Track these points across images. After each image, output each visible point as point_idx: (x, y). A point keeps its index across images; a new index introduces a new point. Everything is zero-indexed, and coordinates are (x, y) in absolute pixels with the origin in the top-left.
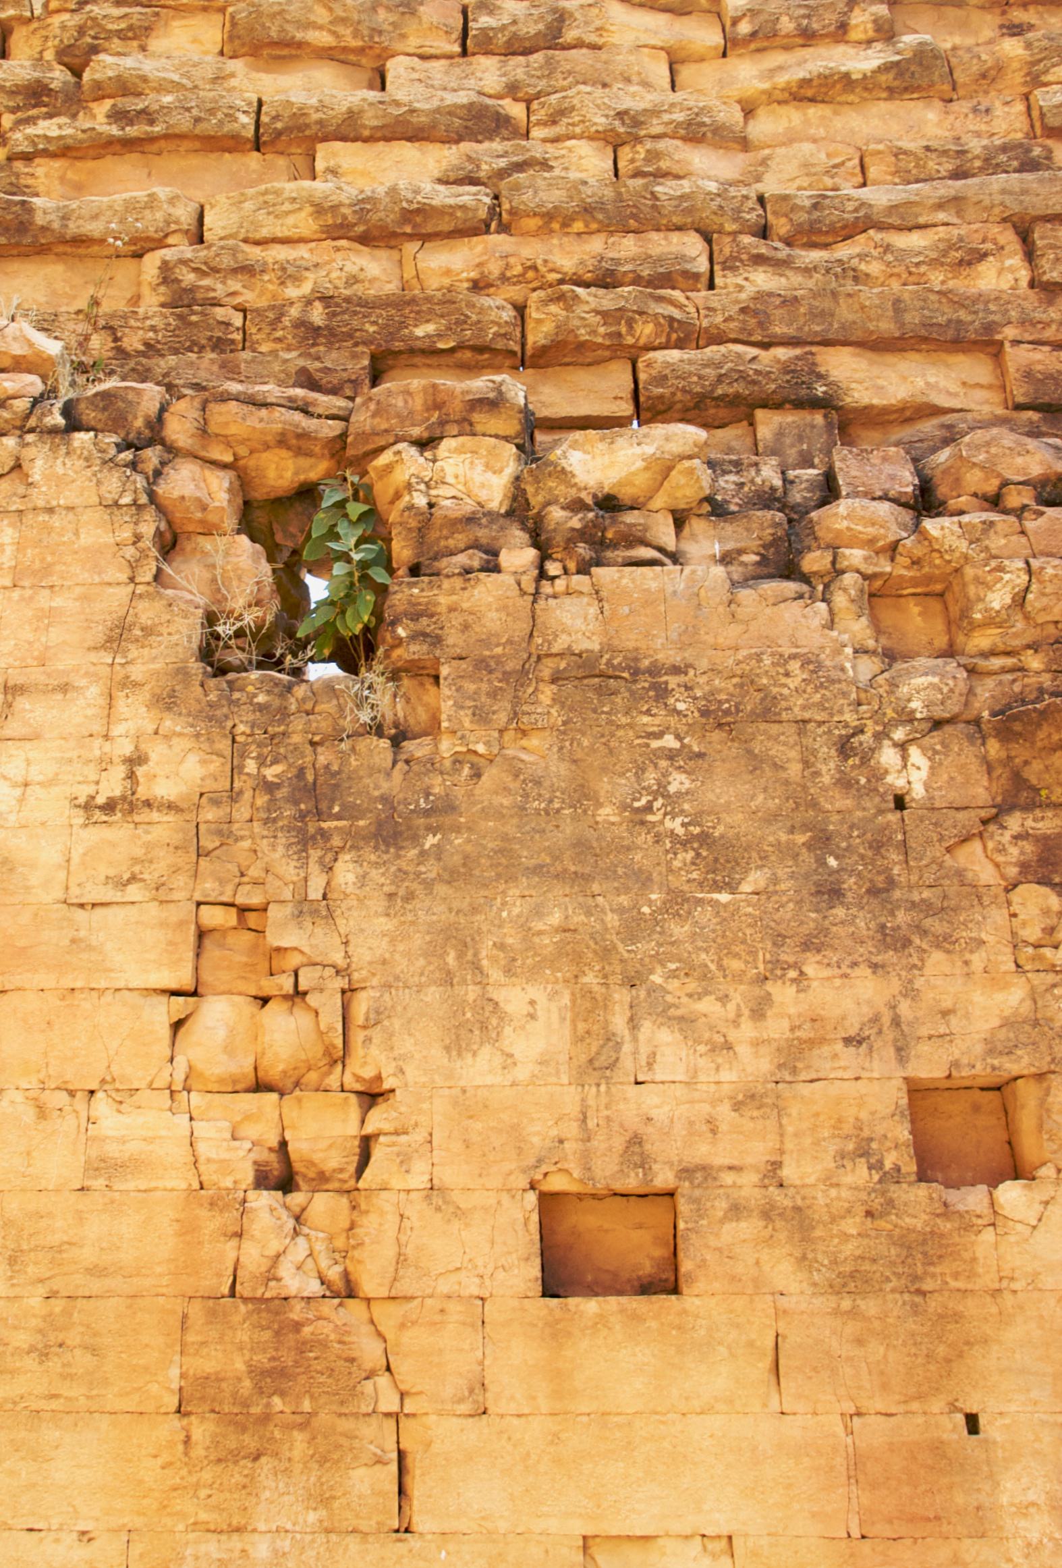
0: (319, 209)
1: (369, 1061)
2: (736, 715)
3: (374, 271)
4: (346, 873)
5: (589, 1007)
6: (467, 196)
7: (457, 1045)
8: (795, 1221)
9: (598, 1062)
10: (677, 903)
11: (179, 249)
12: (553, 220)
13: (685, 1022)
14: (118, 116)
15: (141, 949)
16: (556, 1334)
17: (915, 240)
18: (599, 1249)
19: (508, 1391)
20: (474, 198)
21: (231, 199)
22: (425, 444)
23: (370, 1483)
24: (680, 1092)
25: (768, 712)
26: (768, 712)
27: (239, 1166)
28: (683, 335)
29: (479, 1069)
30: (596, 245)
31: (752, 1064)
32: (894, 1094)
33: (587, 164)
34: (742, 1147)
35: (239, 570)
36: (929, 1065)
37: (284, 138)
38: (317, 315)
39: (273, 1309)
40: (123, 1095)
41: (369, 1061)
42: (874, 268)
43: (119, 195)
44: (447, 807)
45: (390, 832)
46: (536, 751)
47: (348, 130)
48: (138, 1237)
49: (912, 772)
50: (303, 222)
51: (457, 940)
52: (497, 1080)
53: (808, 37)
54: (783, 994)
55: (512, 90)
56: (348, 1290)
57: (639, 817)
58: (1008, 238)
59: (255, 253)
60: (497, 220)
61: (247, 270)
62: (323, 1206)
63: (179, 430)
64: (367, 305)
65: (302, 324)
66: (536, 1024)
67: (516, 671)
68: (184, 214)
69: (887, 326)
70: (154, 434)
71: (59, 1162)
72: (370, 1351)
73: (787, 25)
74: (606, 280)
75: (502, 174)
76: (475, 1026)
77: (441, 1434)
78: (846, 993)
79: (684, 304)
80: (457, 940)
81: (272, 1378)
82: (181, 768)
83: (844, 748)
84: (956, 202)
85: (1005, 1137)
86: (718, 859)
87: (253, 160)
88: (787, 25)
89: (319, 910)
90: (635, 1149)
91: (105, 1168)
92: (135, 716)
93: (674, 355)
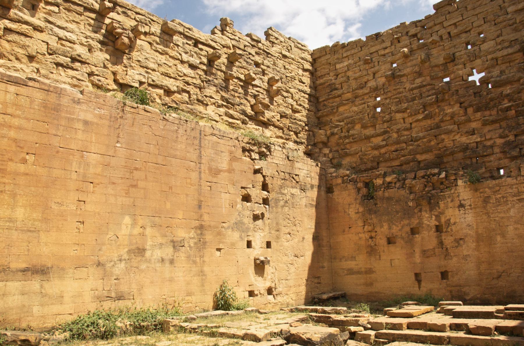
0: (371, 147)
1: (376, 229)
2: (398, 201)
3: (376, 152)
4: (373, 216)
5: (389, 224)
6: (384, 143)
7: (381, 228)
8: (403, 238)
9: (390, 228)
10: (395, 216)
11: (360, 153)
12: (392, 145)
13: (395, 225)
14: (353, 139)
15: (360, 223)
16: (388, 247)
17: (425, 140)
18: (390, 241)
19: (385, 251)
20: (384, 143)
21: (364, 147)
22: (376, 179)
23: (378, 257)
24: (395, 230)
25: (400, 200)
26: (400, 200)
27: (368, 237)
28: (403, 156)
29: (382, 229)
30: (396, 146)
31: (400, 227)
32: (409, 229)
33: (395, 135)
34: (399, 234)
35: (364, 191)
36: (412, 227)
37: (368, 138)
38: (372, 159)
39: (371, 247)
40: (361, 233)
41: (376, 229)
42: (421, 144)
43: (355, 148)
44: (379, 210)
45: (375, 212)
46: (385, 205)
47: (373, 136)
48: (363, 242)
49: (411, 204)
50: (370, 149)
51: (380, 220)
52: (384, 230)
53: (415, 114)
54: (402, 222)
55: (388, 127)
56: (376, 245)
57: (392, 210)
58: (434, 138)
59: (366, 153)
60: (387, 145)
61: (366, 155)
62: (374, 239)
63: (358, 180)
64: (376, 157)
65: (371, 160)
66: (386, 226)
67: (383, 199)
68: (360, 149)
69: (421, 152)
70: (356, 181)
71: (357, 238)
72: (377, 249)
73: (413, 114)
74: (397, 151)
75: (387, 139)
76: (382, 226)
77: (382, 254)
78: (406, 222)
79: (403, 152)
80: (380, 220)
81: (371, 251)
82: (361, 210)
83: (406, 203)
84: (429, 135)
85: (20, 274)
86: (397, 212)
87: (365, 141)
88: (413, 114)
89: (371, 219)
90: (393, 234)
91: (360, 238)
92: (358, 206)
93: (402, 158)
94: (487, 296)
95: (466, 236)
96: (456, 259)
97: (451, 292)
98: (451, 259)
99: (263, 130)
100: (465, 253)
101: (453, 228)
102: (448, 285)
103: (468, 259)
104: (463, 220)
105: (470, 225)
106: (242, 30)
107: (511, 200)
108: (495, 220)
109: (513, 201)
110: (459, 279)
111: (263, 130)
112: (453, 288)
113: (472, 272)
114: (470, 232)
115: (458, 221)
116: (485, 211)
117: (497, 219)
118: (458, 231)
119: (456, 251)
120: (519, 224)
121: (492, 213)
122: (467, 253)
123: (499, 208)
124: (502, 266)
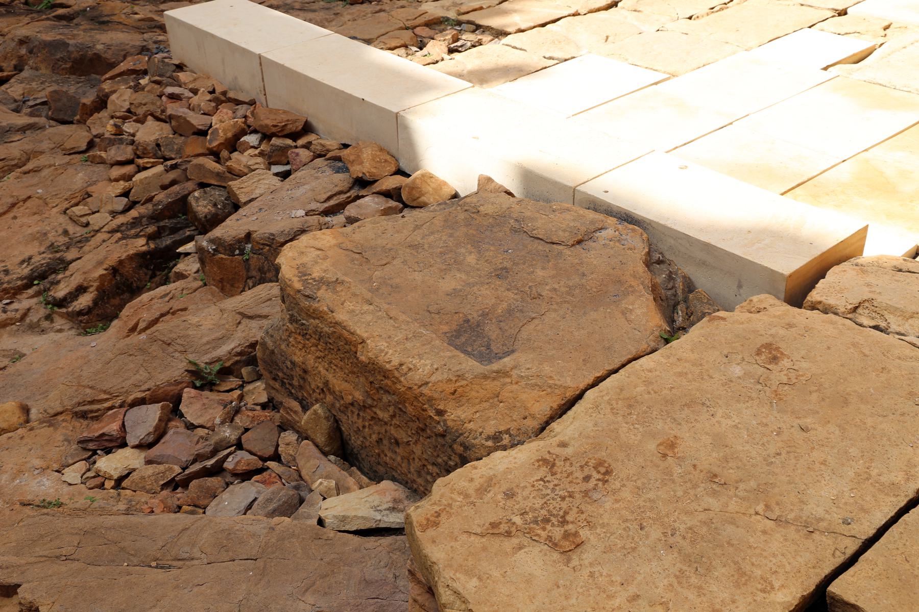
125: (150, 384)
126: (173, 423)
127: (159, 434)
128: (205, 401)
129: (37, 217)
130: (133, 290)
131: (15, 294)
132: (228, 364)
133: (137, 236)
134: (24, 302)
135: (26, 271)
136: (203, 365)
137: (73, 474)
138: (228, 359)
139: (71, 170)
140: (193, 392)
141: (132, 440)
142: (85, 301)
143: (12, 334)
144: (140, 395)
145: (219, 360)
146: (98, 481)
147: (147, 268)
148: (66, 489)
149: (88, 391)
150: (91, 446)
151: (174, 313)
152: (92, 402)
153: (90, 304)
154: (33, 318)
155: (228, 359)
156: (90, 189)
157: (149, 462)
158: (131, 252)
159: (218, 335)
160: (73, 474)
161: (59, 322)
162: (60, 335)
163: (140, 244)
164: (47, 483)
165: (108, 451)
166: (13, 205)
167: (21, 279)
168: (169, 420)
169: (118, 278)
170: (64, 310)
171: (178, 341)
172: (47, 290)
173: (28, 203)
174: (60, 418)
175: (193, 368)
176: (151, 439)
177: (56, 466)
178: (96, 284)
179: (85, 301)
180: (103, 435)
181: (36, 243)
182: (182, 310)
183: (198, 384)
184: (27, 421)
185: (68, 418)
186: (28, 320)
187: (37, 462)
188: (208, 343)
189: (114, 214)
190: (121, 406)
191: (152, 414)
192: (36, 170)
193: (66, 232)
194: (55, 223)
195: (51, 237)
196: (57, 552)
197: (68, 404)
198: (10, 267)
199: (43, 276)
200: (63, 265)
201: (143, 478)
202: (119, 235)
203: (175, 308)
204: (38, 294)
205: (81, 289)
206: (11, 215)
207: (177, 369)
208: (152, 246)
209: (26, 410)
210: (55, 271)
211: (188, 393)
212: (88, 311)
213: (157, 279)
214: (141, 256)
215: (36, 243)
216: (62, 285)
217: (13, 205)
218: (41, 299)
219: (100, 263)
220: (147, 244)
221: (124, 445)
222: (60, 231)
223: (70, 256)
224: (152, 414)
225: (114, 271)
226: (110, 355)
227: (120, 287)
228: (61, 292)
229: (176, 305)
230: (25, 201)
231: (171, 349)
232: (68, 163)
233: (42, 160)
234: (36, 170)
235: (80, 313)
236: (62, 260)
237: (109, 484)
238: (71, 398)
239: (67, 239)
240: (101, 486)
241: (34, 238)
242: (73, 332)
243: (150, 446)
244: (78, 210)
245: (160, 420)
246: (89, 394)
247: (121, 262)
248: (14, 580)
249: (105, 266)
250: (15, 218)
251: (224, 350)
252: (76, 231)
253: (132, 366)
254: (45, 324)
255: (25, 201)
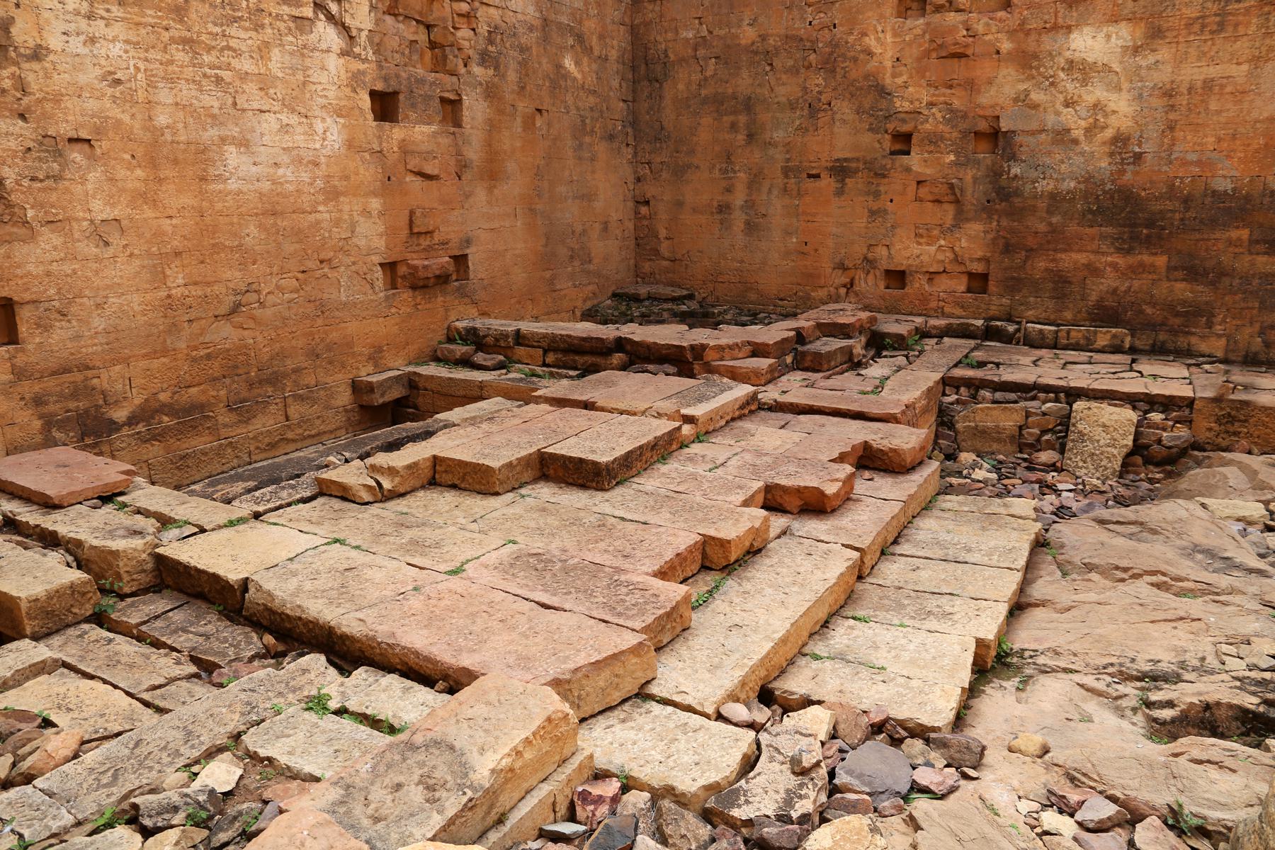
94: (193, 390)
95: (98, 130)
96: (57, 240)
97: (38, 401)
98: (33, 236)
99: (837, 480)
100: (100, 210)
101: (32, 74)
102: (20, 374)
103: (116, 240)
104: (76, 45)
105: (118, 82)
106: (977, 526)
107: (274, 12)
108: (219, 80)
109: (278, 17)
110: (78, 337)
111: (837, 480)
112: (50, 383)
113: (136, 298)
114: (116, 112)
115: (55, 42)
116: (178, 31)
117: (226, 75)
118: (57, 99)
119: (54, 197)
120: (293, 111)
121: (210, 49)
122: (108, 214)
123: (233, 30)
124: (243, 265)
125: (1133, 794)
126: (1120, 830)
127: (1100, 828)
128: (1161, 836)
129: (1192, 636)
130: (1214, 731)
131: (1126, 679)
132: (1210, 828)
133: (1254, 694)
134: (1129, 689)
135: (1147, 667)
136: (1186, 811)
137: (1025, 806)
138: (1214, 825)
139: (1252, 617)
140: (1158, 822)
141: (1079, 816)
142: (1167, 714)
143: (1099, 704)
144: (1119, 794)
145: (1204, 818)
146: (1036, 823)
147: (1243, 723)
148: (1013, 811)
149: (1089, 765)
150: (1053, 799)
151: (1221, 767)
152: (1085, 775)
153: (1168, 719)
154: (1124, 703)
155: (1214, 825)
156: (1252, 639)
157: (1075, 839)
158: (1235, 702)
159: (1223, 800)
160: (1025, 806)
161: (1139, 718)
162: (1131, 726)
163: (1250, 702)
164: (1005, 797)
165: (1061, 812)
166: (1182, 619)
167: (1138, 671)
168: (1119, 825)
169: (1207, 714)
170: (1147, 711)
171: (1184, 781)
172: (1149, 690)
173: (1194, 624)
174: (1056, 768)
175: (1176, 808)
176: (1091, 825)
177: (1021, 794)
178: (1183, 707)
179: (1167, 714)
180: (1064, 797)
181: (1173, 654)
182: (1230, 770)
183: (1170, 822)
184: (1040, 757)
185: (1061, 773)
186: (1119, 702)
187: (1016, 783)
188: (1208, 800)
189: (1252, 667)
190: (1101, 792)
191: (1108, 810)
192: (1224, 604)
193: (1203, 659)
194: (1205, 646)
195: (1188, 656)
196: (959, 833)
197: (1069, 764)
198: (1138, 659)
199: (1155, 679)
200: (1173, 678)
201: (1059, 844)
202: (1238, 684)
203: (1226, 764)
204: (1142, 689)
205: (1170, 704)
206: (1174, 624)
207: (1163, 798)
208: (1261, 709)
209: (1046, 750)
210: (1166, 681)
211: (1153, 821)
212: (1164, 723)
213: (1248, 739)
214: (1245, 711)
215: (1173, 654)
216: (1161, 693)
217: (1182, 619)
218: (1140, 693)
219: (1200, 694)
220: (1258, 705)
221: (1072, 815)
222: (1200, 655)
223: (1187, 676)
224: (1110, 810)
225: (1207, 707)
226: (1127, 754)
227: (1206, 720)
228: (1154, 697)
229: (1229, 762)
230: (1193, 620)
231: (1172, 781)
232: (1256, 611)
233: (1237, 599)
234: (1224, 604)
235: (1155, 720)
236: (1178, 676)
237: (1038, 830)
238: (1074, 761)
239: (1198, 664)
240: (1033, 828)
241: (1175, 649)
242: (1142, 731)
243: (1089, 830)
244: (1225, 648)
245: (1109, 818)
246: (1088, 768)
247: (1218, 704)
248: (923, 825)
249: (1202, 698)
250: (1175, 628)
251: (1214, 815)
252: (1212, 662)
253: (1134, 772)
254: (1129, 713)
255: (1193, 620)
